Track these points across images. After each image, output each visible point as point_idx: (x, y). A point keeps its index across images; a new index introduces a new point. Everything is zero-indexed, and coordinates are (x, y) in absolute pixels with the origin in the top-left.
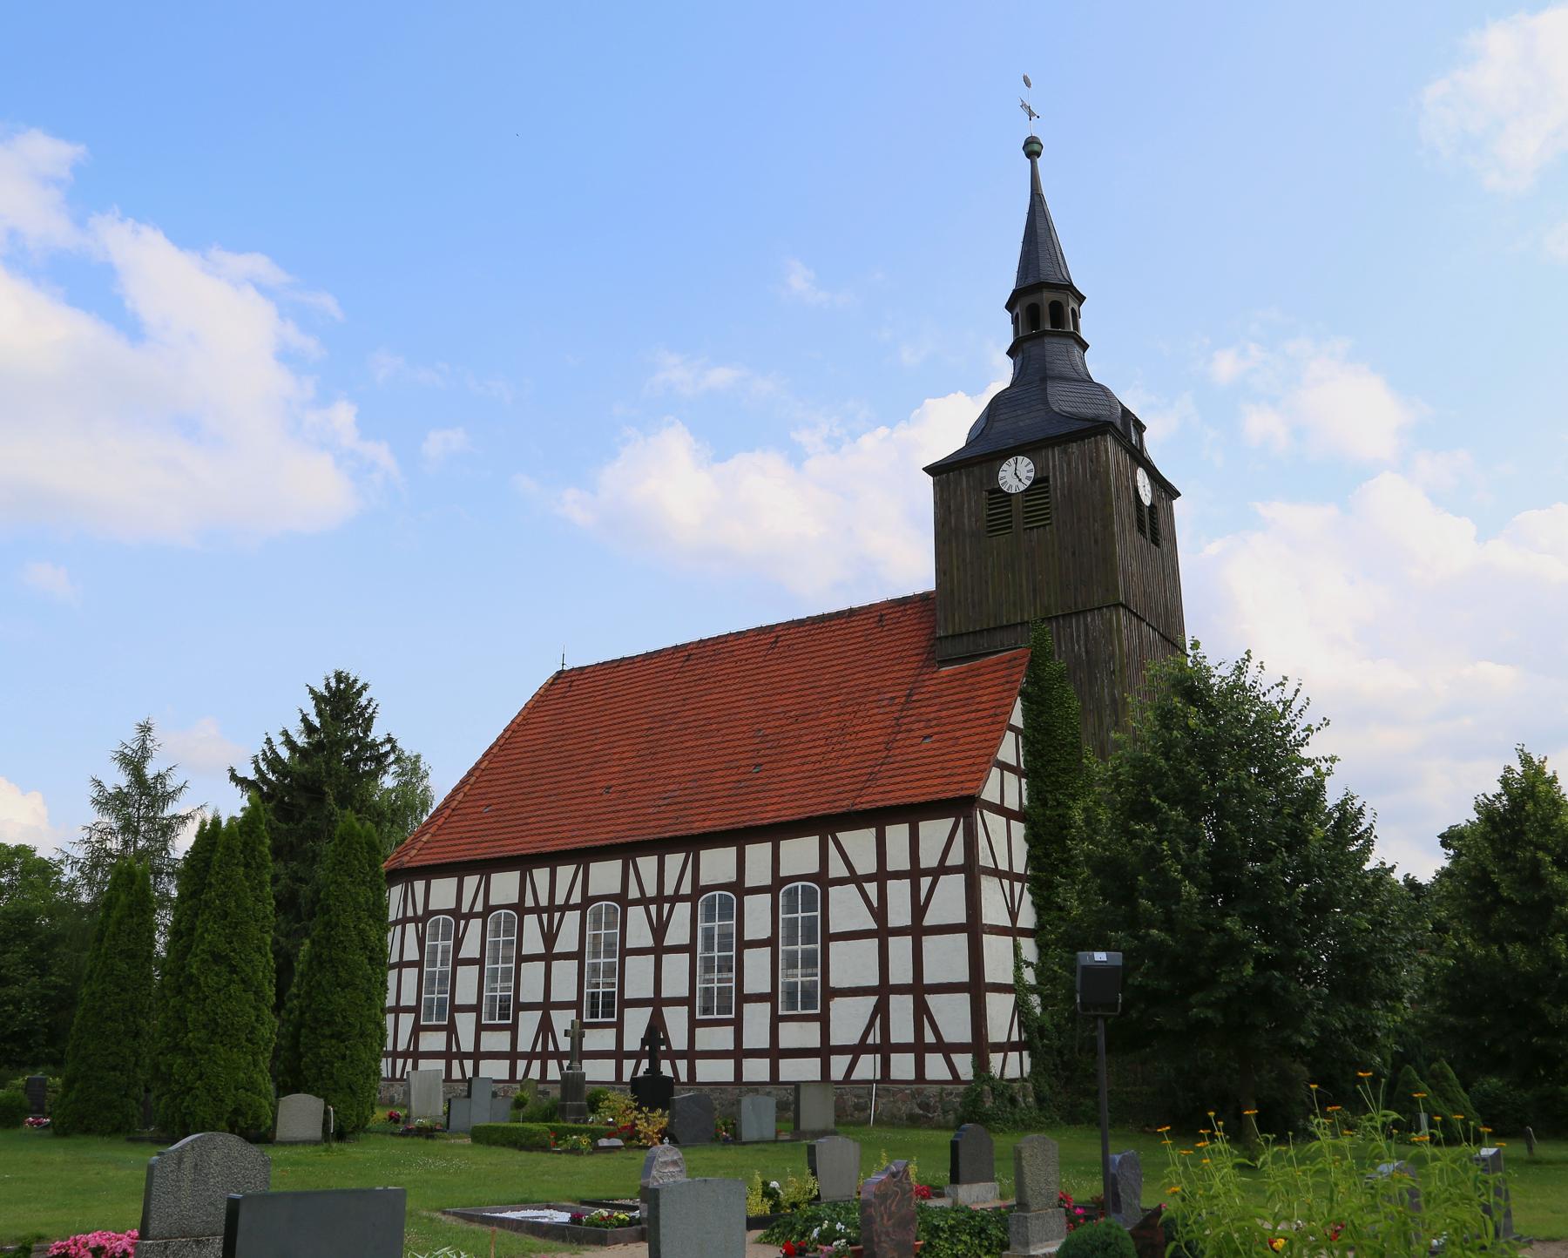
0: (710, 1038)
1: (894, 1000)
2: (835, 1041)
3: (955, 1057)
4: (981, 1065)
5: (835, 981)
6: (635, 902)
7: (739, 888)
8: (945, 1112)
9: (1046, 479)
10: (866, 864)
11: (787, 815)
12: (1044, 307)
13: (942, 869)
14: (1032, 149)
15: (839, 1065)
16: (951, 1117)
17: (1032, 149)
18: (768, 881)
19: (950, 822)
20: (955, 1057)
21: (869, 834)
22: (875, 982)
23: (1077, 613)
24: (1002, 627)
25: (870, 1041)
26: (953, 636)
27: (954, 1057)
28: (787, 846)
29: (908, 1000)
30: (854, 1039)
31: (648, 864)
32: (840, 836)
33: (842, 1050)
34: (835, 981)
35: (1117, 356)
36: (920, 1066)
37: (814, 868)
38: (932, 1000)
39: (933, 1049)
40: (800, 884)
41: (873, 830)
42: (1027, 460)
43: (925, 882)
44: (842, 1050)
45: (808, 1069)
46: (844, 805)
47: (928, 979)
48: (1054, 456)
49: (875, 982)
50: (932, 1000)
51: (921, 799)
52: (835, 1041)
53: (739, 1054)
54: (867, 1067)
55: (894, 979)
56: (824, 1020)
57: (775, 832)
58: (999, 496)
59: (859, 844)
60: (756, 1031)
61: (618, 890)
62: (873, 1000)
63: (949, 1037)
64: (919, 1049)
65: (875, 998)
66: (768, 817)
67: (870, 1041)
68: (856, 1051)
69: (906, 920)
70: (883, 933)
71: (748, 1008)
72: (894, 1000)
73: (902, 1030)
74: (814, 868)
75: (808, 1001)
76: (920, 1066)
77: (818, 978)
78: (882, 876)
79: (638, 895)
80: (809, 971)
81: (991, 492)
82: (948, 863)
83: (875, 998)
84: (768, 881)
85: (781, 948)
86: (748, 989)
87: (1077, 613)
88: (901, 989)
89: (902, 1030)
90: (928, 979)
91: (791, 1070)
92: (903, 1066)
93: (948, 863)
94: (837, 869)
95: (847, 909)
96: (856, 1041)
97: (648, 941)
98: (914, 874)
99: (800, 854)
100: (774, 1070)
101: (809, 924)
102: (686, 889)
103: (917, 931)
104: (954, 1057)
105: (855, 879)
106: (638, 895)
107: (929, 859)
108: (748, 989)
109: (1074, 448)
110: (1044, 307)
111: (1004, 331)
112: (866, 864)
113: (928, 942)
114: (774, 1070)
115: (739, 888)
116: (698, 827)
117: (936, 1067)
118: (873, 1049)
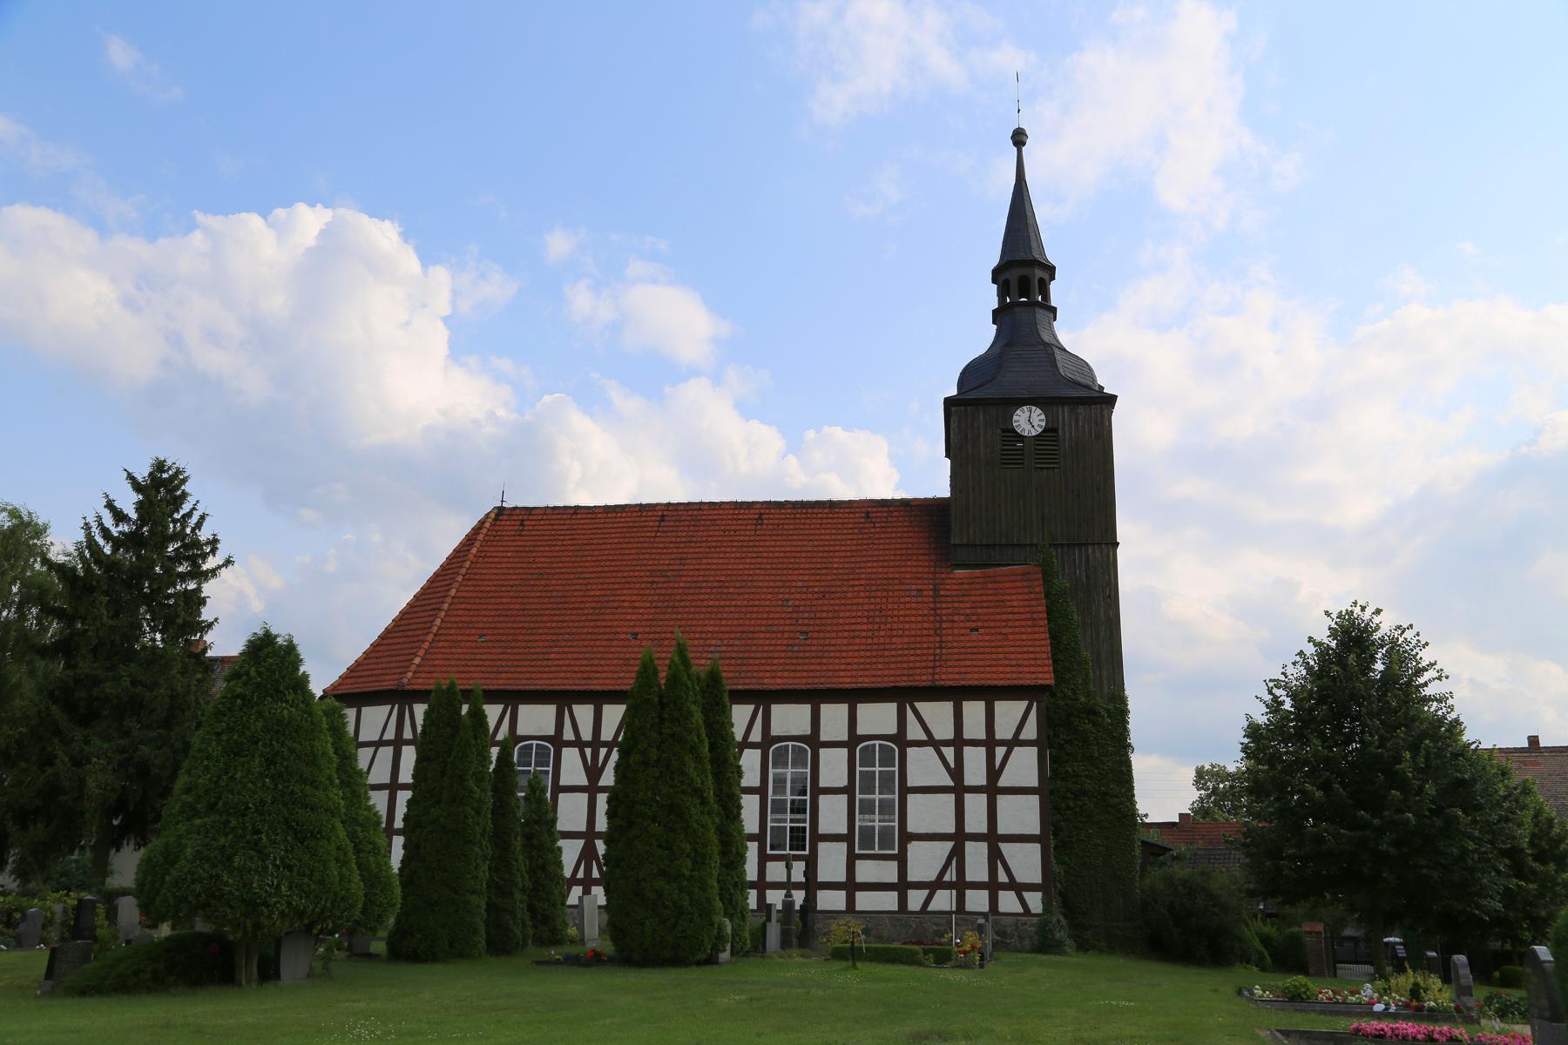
0: (867, 871)
1: (970, 846)
2: (912, 876)
3: (1027, 895)
4: (810, 900)
5: (912, 827)
6: (569, 744)
7: (814, 741)
8: (1021, 938)
9: (1055, 430)
10: (944, 731)
11: (865, 682)
12: (1023, 277)
13: (1015, 742)
14: (1019, 138)
15: (916, 899)
16: (1027, 942)
17: (1019, 138)
18: (844, 737)
19: (1023, 705)
20: (1027, 895)
21: (948, 707)
22: (952, 830)
23: (1080, 545)
24: (1013, 545)
25: (947, 878)
26: (967, 545)
27: (1025, 894)
28: (864, 710)
29: (983, 847)
30: (931, 876)
31: (584, 713)
32: (918, 705)
33: (919, 885)
34: (912, 827)
35: (1083, 330)
36: (994, 901)
37: (892, 729)
38: (1005, 848)
39: (1005, 887)
40: (877, 743)
41: (895, 705)
42: (1039, 411)
43: (1000, 752)
44: (919, 885)
45: (889, 901)
46: (924, 680)
47: (1001, 831)
48: (1064, 413)
49: (952, 830)
50: (1006, 848)
51: (599, 688)
52: (912, 876)
53: (902, 886)
54: (943, 901)
55: (970, 828)
56: (902, 860)
57: (853, 696)
58: (1012, 435)
59: (938, 715)
60: (831, 863)
61: (552, 732)
62: (950, 845)
63: (1021, 877)
64: (993, 887)
65: (582, 842)
66: (846, 682)
67: (947, 878)
68: (933, 887)
69: (981, 780)
70: (959, 789)
71: (823, 847)
72: (970, 846)
73: (977, 869)
74: (892, 729)
75: (886, 841)
76: (994, 901)
77: (896, 824)
78: (959, 742)
79: (573, 738)
80: (798, 816)
81: (1004, 431)
82: (1022, 737)
83: (582, 842)
84: (844, 737)
85: (858, 796)
86: (823, 829)
87: (1080, 545)
88: (976, 837)
89: (977, 869)
90: (1001, 831)
91: (865, 901)
92: (977, 901)
93: (1022, 737)
94: (914, 732)
95: (924, 767)
96: (933, 878)
97: (582, 780)
98: (990, 743)
99: (878, 718)
100: (851, 901)
101: (886, 779)
102: (756, 736)
103: (992, 790)
104: (1025, 894)
105: (578, 743)
106: (573, 738)
107: (1004, 731)
108: (823, 829)
109: (1081, 409)
110: (1023, 277)
111: (990, 297)
112: (944, 731)
113: (1002, 800)
114: (851, 901)
115: (814, 741)
116: (769, 684)
117: (1008, 902)
118: (949, 886)
